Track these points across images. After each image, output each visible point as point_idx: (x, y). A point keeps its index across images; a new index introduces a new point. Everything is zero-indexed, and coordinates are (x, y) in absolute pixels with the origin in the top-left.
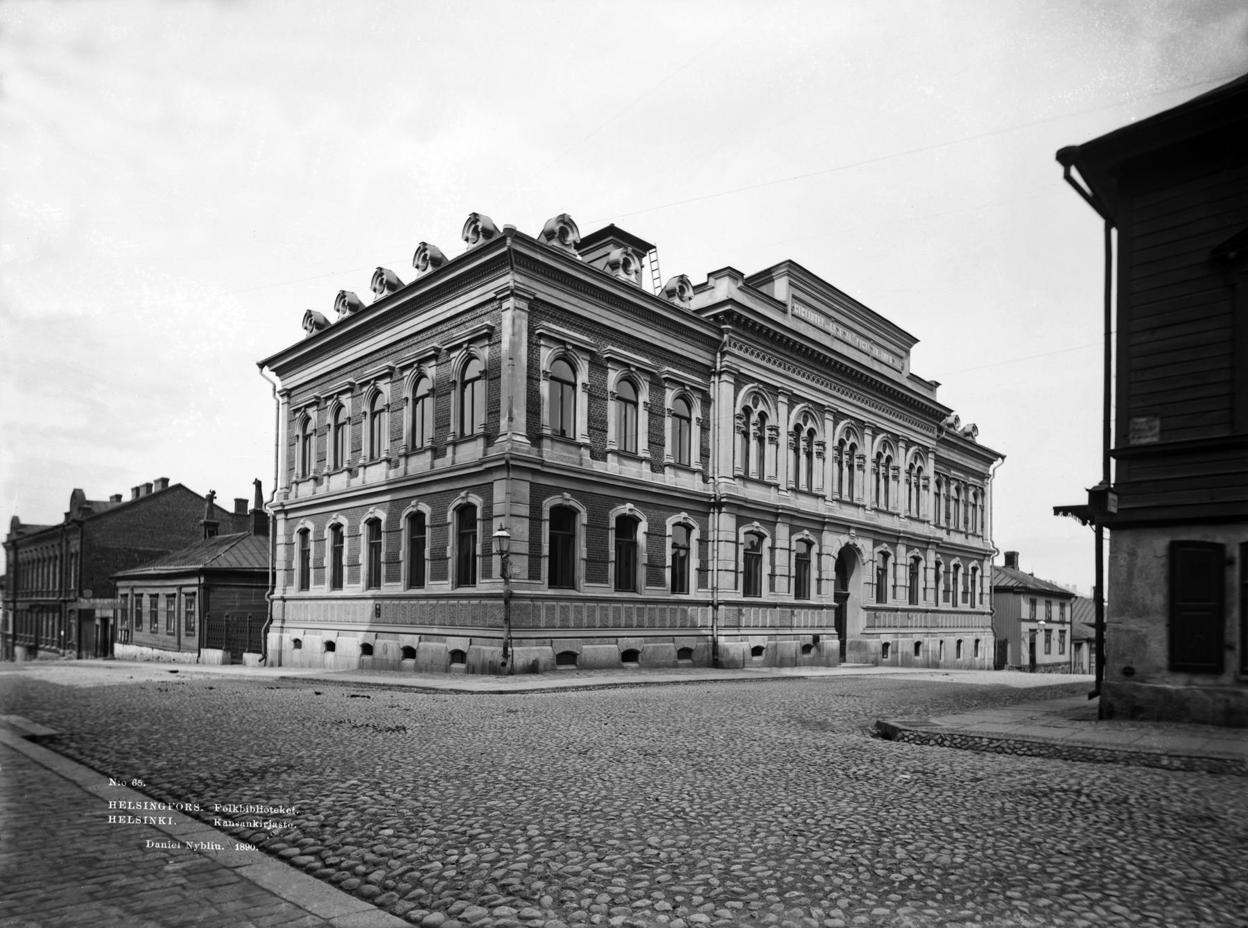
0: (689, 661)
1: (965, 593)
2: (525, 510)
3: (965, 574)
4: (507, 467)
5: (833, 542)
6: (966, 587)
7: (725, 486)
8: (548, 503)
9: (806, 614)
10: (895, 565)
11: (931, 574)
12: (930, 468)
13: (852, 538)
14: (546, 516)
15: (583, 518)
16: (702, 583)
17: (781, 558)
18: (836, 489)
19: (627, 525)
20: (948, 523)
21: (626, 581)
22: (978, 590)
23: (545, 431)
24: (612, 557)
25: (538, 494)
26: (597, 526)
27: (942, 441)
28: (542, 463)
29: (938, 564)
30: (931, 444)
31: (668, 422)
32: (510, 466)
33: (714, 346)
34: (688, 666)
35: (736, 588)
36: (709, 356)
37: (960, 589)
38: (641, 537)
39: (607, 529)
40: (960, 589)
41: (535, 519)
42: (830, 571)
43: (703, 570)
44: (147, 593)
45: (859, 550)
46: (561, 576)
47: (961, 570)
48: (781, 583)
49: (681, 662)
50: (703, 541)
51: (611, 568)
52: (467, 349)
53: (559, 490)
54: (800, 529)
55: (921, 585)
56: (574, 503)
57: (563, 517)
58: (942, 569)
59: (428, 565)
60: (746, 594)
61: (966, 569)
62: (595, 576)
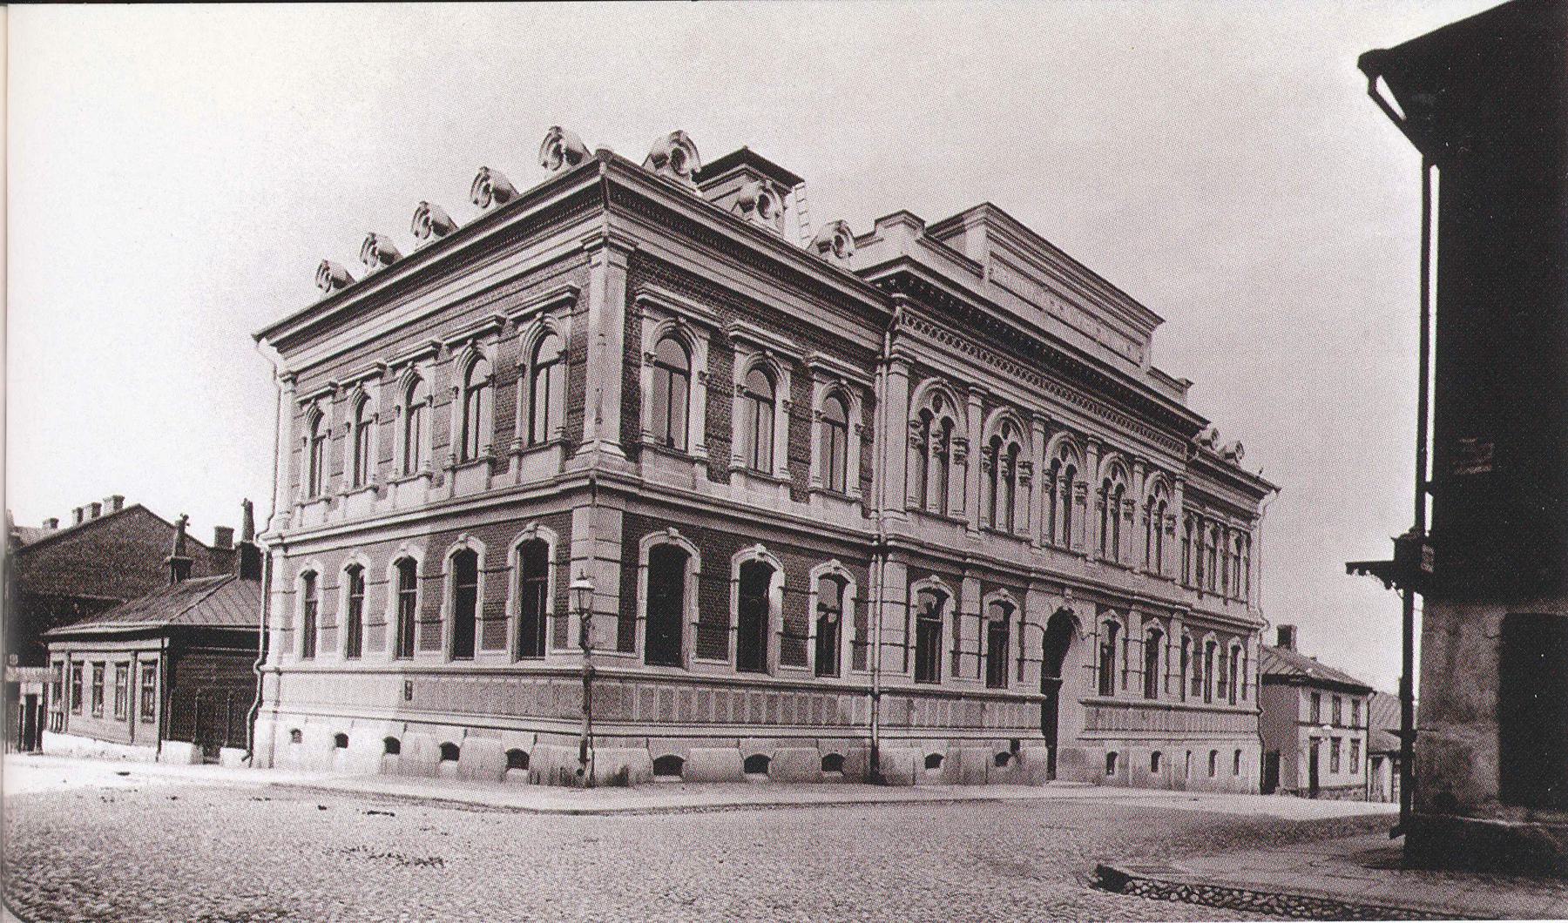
0: (838, 774)
1: (1222, 683)
2: (615, 552)
3: (1223, 657)
4: (592, 489)
5: (1041, 608)
6: (1223, 675)
7: (891, 524)
8: (647, 543)
9: (944, 707)
10: (1245, 660)
11: (1176, 655)
12: (1176, 503)
13: (1067, 601)
14: (644, 560)
15: (695, 564)
16: (859, 662)
17: (969, 627)
18: (985, 512)
19: (757, 575)
20: (1200, 583)
21: (752, 658)
22: (1240, 680)
23: (645, 439)
24: (735, 622)
25: (633, 528)
26: (714, 578)
27: (1194, 466)
28: (641, 485)
29: (1185, 641)
30: (1179, 469)
31: (816, 430)
32: (596, 488)
33: (881, 323)
34: (837, 781)
35: (906, 670)
36: (875, 337)
37: (1216, 677)
38: (775, 594)
39: (728, 580)
40: (1216, 677)
41: (629, 565)
42: (1036, 651)
43: (860, 643)
44: (89, 659)
45: (1077, 620)
46: (664, 649)
47: (1217, 651)
48: (969, 664)
49: (826, 775)
50: (861, 602)
51: (733, 638)
52: (541, 320)
53: (663, 525)
54: (995, 587)
55: (1119, 665)
56: (686, 545)
57: (668, 563)
58: (1191, 648)
59: (479, 627)
60: (919, 678)
61: (1224, 649)
62: (712, 646)
